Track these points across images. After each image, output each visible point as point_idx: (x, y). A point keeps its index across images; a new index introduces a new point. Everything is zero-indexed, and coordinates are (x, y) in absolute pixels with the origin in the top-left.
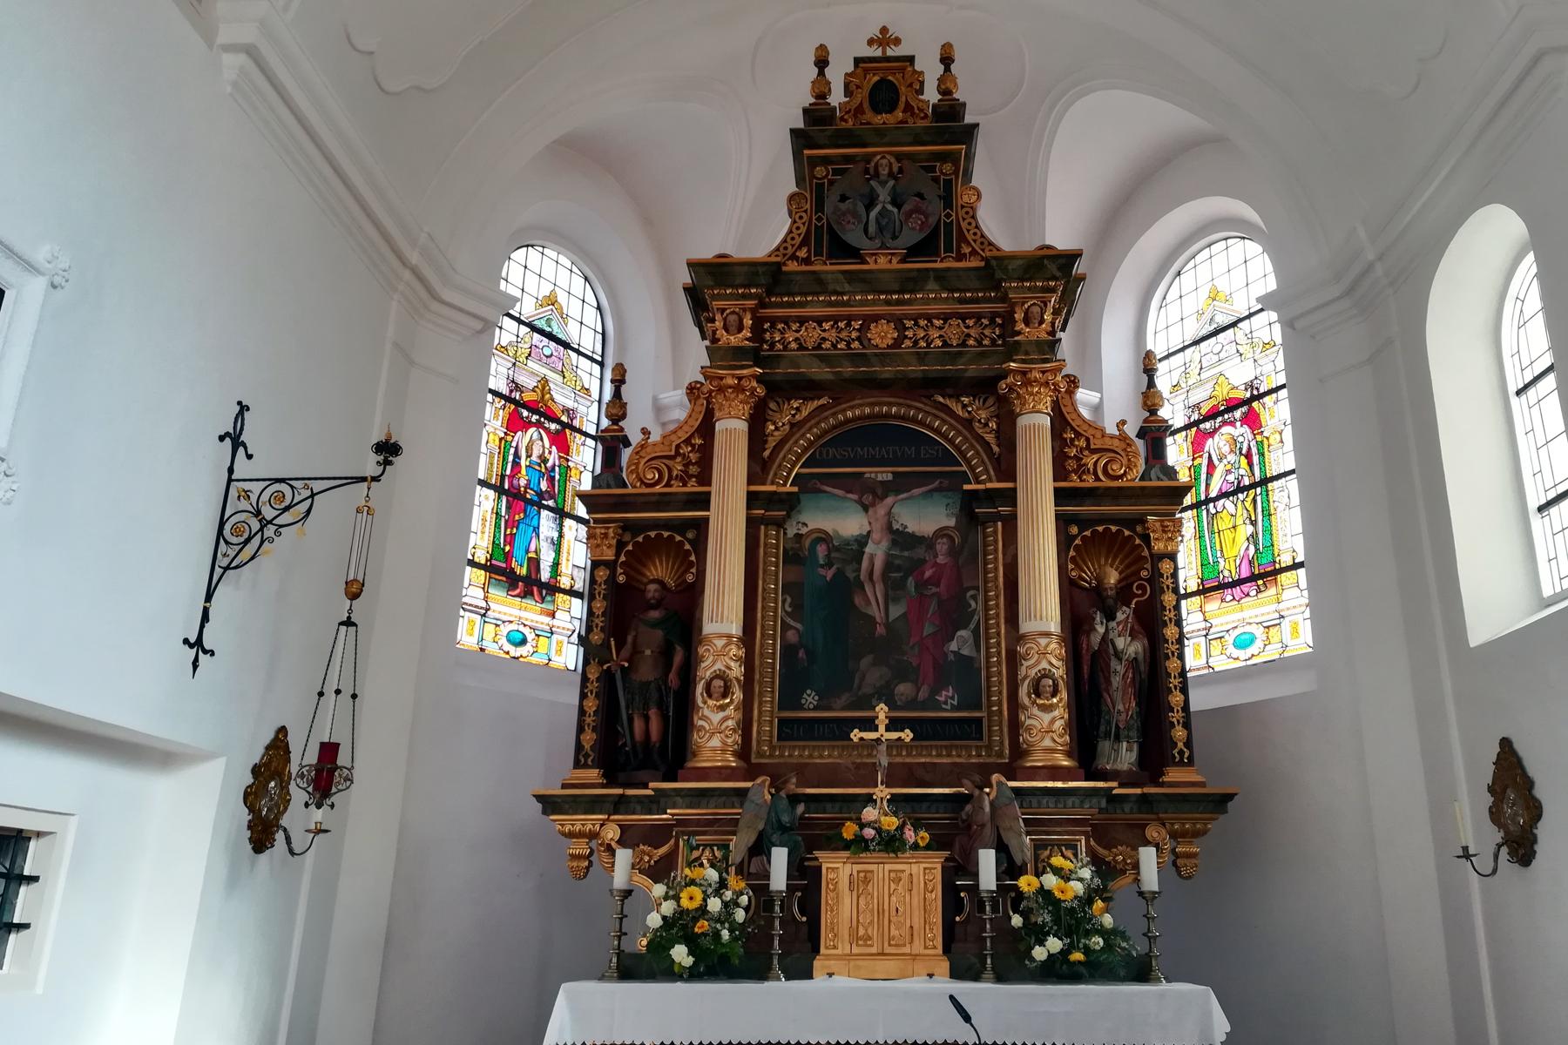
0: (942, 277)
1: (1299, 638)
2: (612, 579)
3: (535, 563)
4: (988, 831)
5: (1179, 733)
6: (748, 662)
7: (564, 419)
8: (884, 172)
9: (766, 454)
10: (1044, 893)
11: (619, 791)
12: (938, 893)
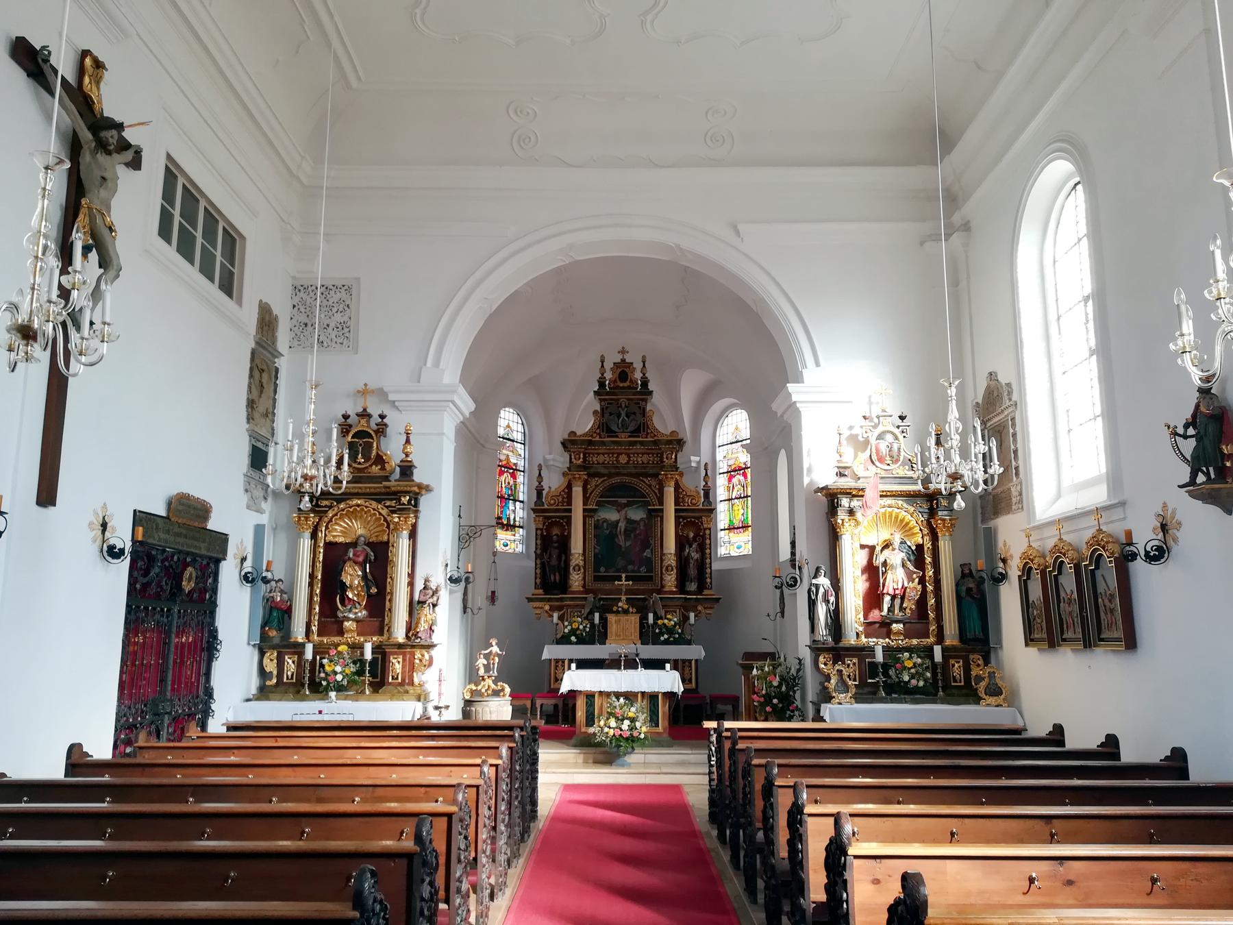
0: (642, 443)
1: (747, 549)
2: (542, 534)
3: (509, 519)
4: (652, 609)
5: (708, 580)
6: (584, 560)
7: (514, 467)
8: (623, 406)
9: (588, 495)
10: (664, 624)
11: (549, 596)
12: (638, 624)
